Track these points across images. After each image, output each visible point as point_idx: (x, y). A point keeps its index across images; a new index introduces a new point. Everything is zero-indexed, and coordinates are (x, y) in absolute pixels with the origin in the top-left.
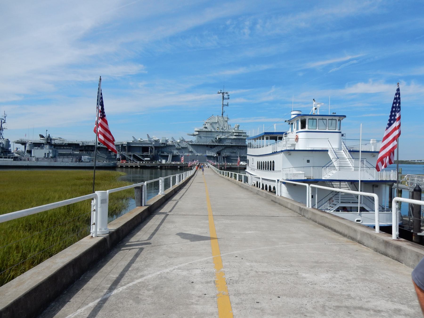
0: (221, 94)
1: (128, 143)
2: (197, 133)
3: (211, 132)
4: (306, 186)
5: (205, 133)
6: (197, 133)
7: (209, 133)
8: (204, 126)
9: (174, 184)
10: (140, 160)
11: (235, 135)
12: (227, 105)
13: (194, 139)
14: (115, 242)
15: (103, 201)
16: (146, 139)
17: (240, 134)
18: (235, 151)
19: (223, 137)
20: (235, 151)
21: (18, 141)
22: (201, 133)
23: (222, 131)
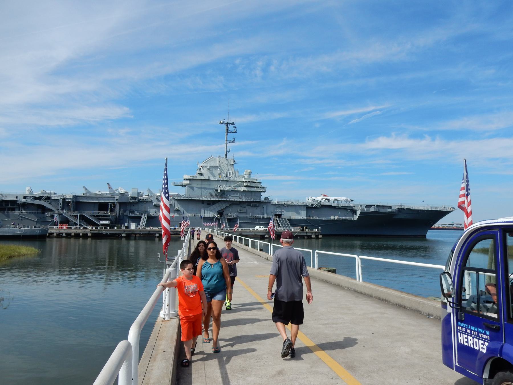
0: (224, 126)
2: (188, 182)
3: (209, 180)
4: (310, 252)
5: (200, 182)
6: (188, 182)
7: (206, 183)
11: (245, 186)
17: (253, 185)
20: (245, 210)
22: (194, 182)
23: (225, 179)
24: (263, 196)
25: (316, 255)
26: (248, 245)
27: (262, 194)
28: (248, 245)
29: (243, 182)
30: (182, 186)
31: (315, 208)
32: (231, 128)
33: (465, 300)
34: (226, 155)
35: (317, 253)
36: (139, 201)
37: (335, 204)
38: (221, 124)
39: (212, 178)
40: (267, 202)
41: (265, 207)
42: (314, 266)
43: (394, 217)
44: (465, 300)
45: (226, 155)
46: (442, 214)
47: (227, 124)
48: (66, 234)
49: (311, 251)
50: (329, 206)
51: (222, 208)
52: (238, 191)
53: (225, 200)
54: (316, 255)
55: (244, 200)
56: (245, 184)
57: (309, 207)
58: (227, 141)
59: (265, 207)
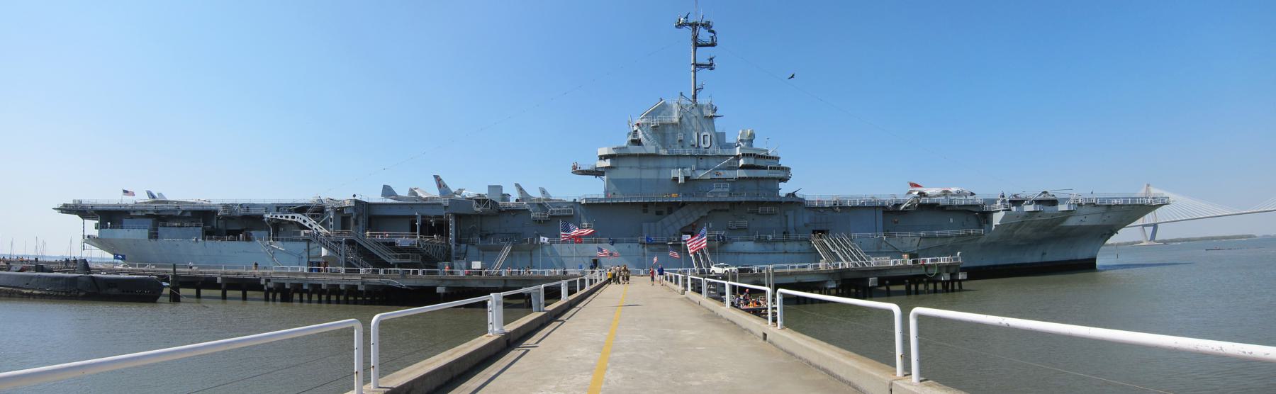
0: (688, 32)
1: (357, 202)
2: (608, 163)
3: (656, 156)
4: (890, 312)
5: (634, 162)
6: (608, 163)
7: (651, 163)
8: (630, 138)
9: (582, 287)
10: (379, 263)
11: (743, 167)
12: (710, 66)
13: (595, 189)
14: (571, 305)
15: (498, 303)
16: (429, 191)
17: (761, 163)
18: (744, 223)
19: (701, 174)
20: (744, 223)
21: (65, 205)
22: (622, 163)
23: (693, 151)
24: (784, 189)
25: (778, 298)
26: (700, 292)
27: (781, 185)
28: (700, 292)
29: (737, 158)
30: (597, 173)
31: (906, 211)
32: (704, 35)
33: (452, 267)
34: (695, 97)
35: (921, 318)
36: (500, 211)
37: (942, 201)
38: (679, 26)
39: (663, 152)
40: (794, 202)
41: (790, 214)
42: (775, 320)
43: (1065, 224)
44: (452, 267)
45: (695, 97)
46: (1134, 210)
47: (695, 26)
48: (310, 285)
49: (895, 308)
50: (933, 208)
51: (691, 221)
52: (725, 180)
53: (698, 200)
54: (778, 298)
55: (743, 199)
56: (742, 162)
57: (891, 212)
58: (696, 65)
59: (790, 214)
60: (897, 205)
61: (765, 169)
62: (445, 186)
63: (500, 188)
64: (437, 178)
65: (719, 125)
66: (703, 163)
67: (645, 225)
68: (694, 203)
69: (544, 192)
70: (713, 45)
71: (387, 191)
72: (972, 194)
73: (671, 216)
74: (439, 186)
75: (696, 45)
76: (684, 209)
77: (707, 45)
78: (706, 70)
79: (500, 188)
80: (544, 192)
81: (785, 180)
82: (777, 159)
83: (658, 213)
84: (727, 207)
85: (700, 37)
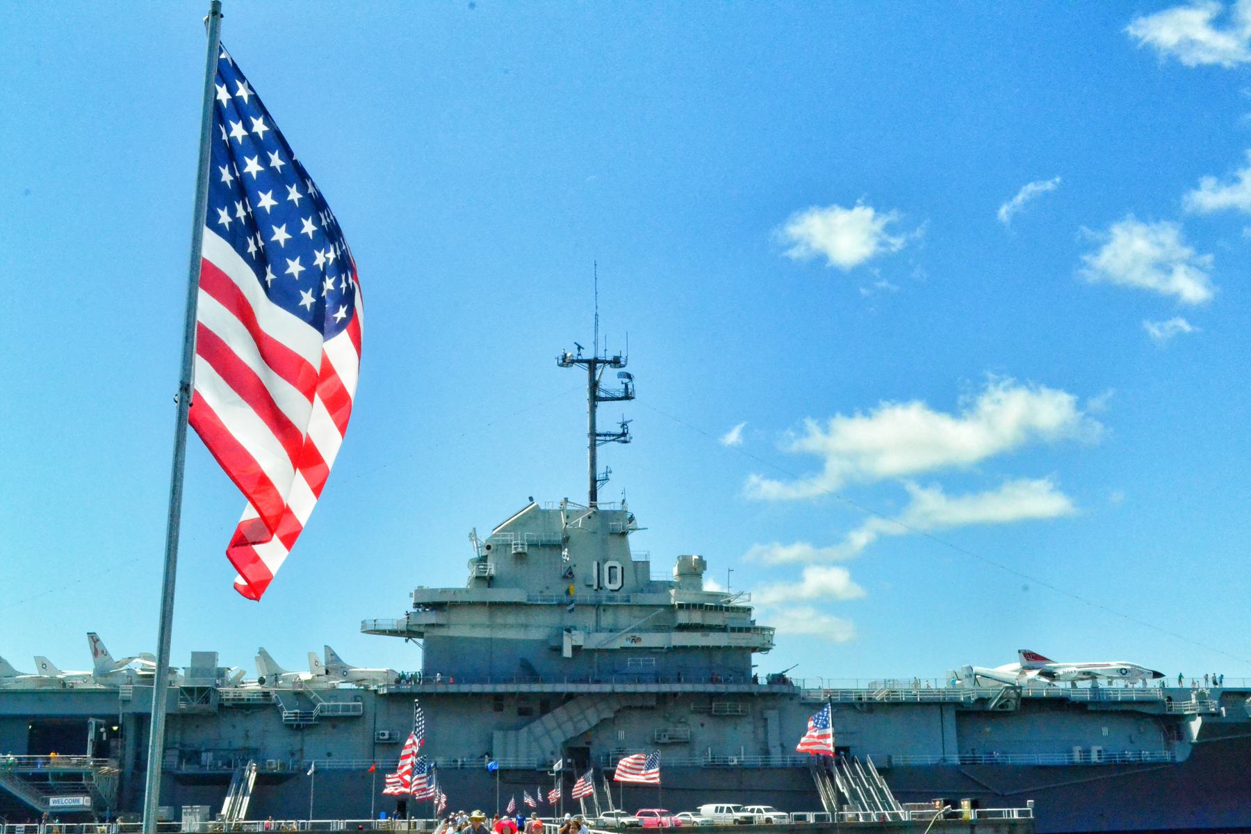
0: (582, 373)
12: (623, 437)
13: (408, 659)
16: (77, 668)
24: (763, 667)
27: (756, 658)
36: (221, 706)
38: (566, 362)
41: (772, 715)
43: (857, 592)
45: (593, 495)
47: (592, 364)
59: (772, 715)
60: (982, 701)
61: (738, 630)
62: (105, 653)
63: (212, 656)
64: (94, 638)
65: (637, 545)
66: (607, 619)
67: (498, 736)
68: (590, 694)
69: (44, 665)
70: (627, 397)
71: (334, 666)
72: (1157, 675)
73: (548, 718)
74: (96, 653)
75: (595, 399)
76: (570, 704)
77: (618, 399)
78: (615, 445)
79: (212, 656)
80: (44, 665)
81: (764, 649)
82: (748, 610)
83: (522, 712)
84: (653, 703)
85: (602, 385)
